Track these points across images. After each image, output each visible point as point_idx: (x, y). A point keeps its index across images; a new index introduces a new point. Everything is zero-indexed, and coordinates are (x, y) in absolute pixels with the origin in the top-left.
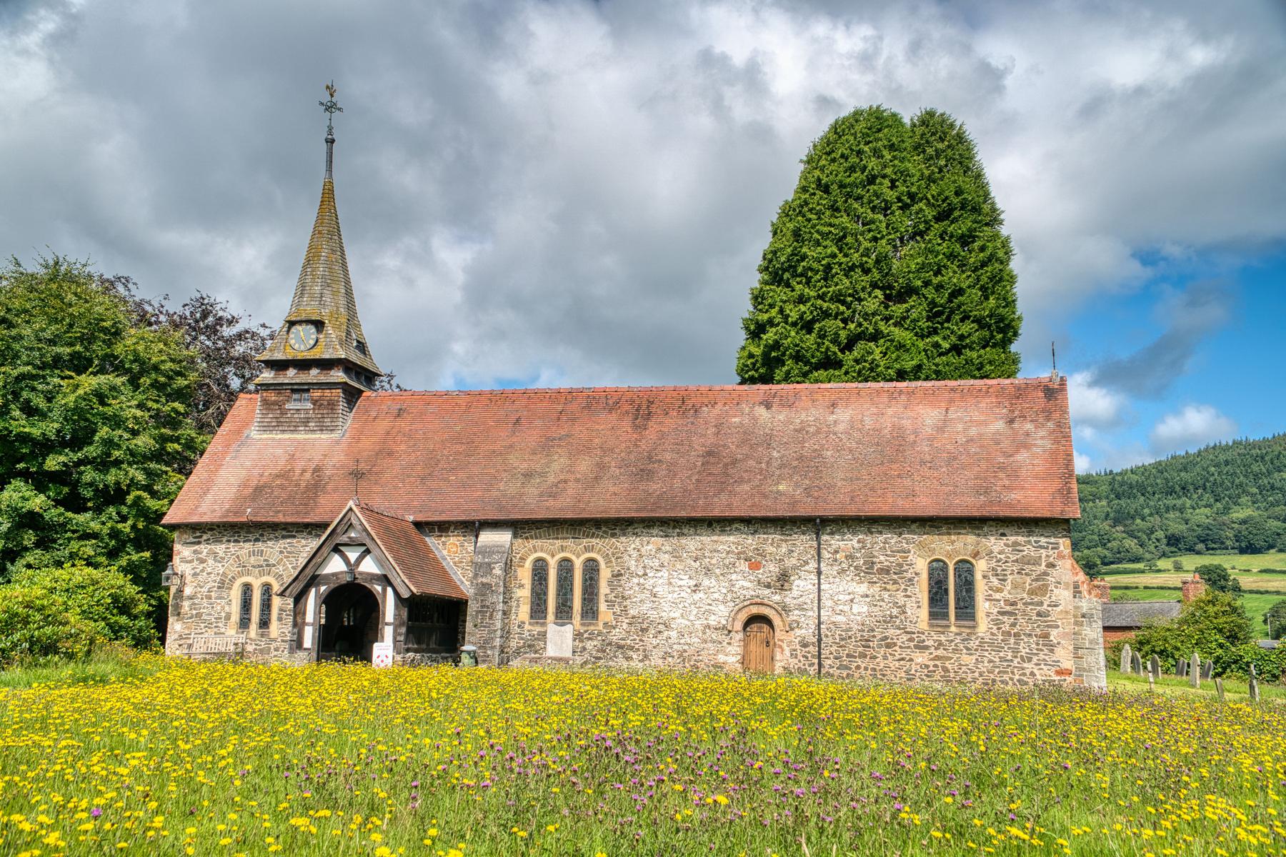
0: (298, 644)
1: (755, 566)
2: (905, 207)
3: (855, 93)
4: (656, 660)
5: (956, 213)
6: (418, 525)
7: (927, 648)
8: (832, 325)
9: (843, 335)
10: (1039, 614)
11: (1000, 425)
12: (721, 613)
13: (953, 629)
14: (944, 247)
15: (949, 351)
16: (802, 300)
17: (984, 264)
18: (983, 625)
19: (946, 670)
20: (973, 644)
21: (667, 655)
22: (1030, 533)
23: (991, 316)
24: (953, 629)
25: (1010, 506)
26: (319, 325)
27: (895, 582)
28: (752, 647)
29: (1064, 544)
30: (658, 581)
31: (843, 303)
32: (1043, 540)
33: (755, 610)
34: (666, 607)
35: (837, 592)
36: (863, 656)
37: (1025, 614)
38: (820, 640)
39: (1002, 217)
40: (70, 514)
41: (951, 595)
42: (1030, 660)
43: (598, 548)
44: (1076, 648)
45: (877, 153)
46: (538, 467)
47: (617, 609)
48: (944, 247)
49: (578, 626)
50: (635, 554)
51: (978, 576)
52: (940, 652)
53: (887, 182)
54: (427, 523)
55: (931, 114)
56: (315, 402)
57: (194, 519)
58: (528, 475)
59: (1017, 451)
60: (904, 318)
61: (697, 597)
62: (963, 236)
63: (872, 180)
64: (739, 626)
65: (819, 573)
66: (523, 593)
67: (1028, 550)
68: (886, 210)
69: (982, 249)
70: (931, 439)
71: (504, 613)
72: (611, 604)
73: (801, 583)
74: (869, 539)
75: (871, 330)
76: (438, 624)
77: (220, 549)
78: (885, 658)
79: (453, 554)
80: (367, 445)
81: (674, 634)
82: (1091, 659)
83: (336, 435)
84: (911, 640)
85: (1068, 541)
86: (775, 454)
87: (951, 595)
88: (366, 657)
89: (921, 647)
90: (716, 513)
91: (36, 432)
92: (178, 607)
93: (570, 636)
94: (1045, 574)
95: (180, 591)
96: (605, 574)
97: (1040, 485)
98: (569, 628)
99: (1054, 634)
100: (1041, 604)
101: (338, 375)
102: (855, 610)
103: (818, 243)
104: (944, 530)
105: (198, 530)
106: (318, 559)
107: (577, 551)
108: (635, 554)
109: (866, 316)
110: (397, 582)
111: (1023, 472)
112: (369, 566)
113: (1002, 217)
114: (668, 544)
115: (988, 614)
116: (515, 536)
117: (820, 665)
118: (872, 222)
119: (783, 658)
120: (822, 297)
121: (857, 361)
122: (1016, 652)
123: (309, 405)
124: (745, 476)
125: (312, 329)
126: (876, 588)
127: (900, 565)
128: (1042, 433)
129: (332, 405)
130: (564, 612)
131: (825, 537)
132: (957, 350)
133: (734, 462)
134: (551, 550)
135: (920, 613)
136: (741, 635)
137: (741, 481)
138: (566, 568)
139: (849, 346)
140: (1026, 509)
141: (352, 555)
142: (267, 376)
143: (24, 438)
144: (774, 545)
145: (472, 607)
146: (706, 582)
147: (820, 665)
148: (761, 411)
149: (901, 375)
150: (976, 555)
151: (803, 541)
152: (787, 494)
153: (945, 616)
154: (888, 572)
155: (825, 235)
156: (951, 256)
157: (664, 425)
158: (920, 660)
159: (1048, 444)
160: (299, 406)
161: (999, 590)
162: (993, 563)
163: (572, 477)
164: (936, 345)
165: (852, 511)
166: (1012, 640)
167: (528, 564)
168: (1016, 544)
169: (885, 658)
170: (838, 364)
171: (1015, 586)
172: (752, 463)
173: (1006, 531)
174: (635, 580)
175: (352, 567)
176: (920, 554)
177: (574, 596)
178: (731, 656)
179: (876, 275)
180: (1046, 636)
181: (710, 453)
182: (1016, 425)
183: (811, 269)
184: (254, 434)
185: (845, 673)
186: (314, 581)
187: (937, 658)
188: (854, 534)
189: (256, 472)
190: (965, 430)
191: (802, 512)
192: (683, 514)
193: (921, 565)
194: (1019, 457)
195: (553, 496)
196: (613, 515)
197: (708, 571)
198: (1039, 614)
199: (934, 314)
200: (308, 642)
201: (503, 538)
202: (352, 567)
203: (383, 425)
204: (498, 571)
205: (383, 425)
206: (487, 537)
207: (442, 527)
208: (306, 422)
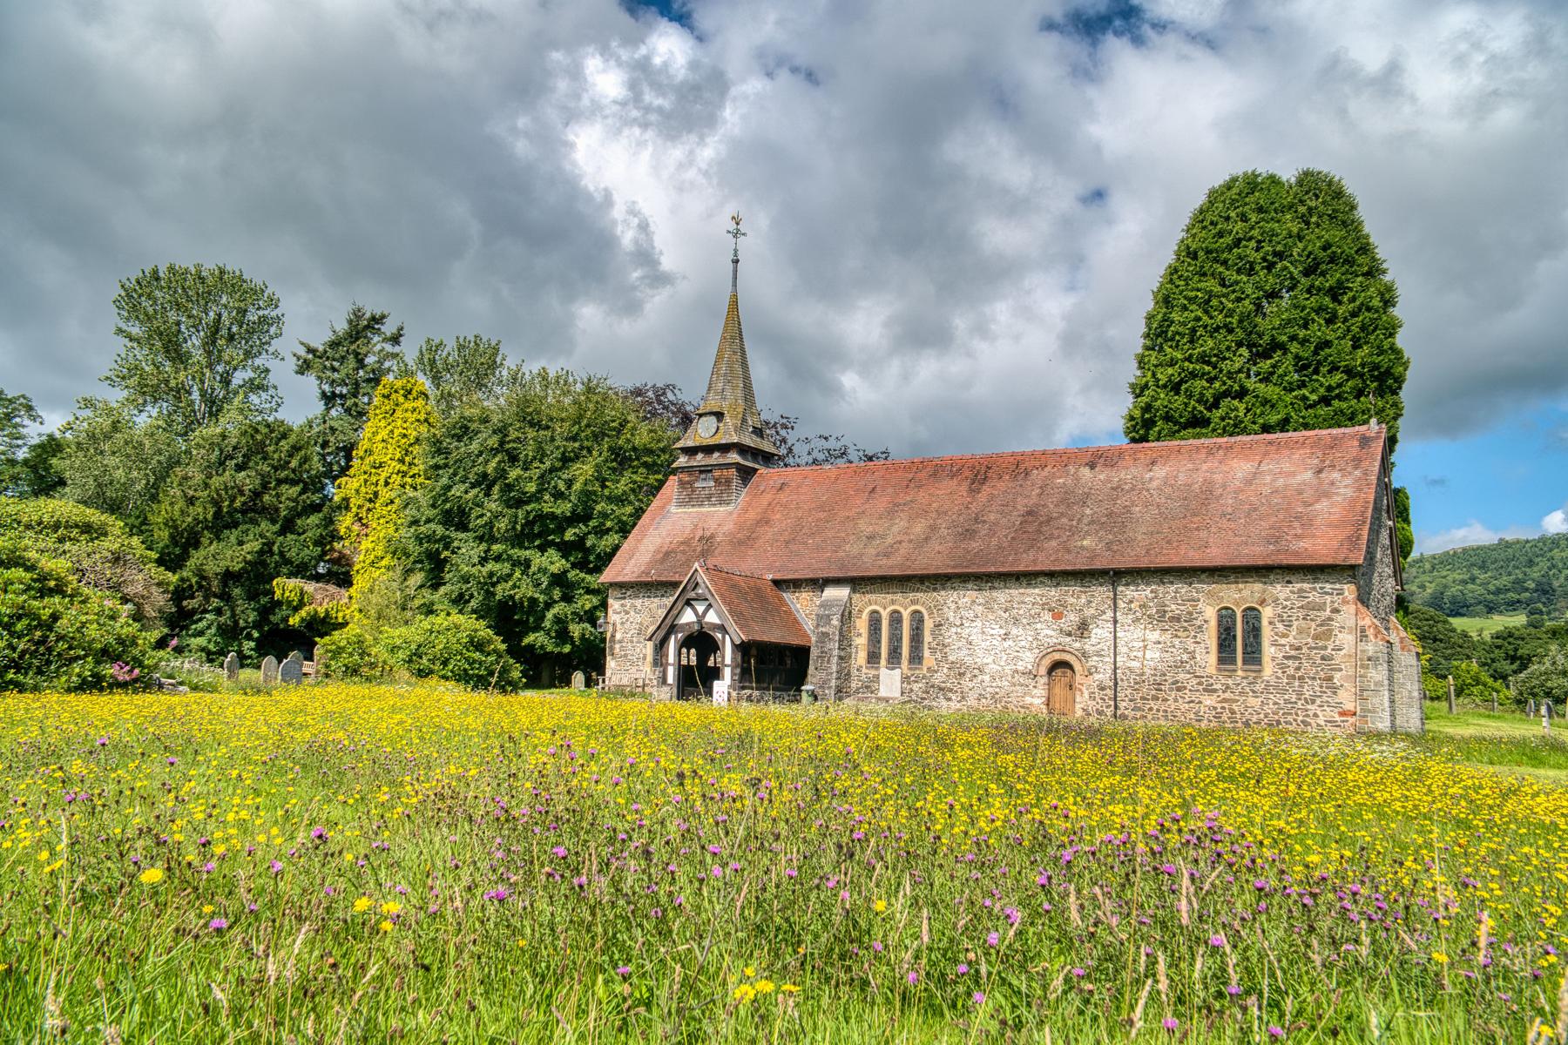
0: (664, 681)
1: (1058, 616)
2: (1270, 267)
3: (1215, 161)
4: (972, 702)
5: (1323, 267)
6: (776, 583)
7: (1215, 691)
8: (1200, 384)
9: (1209, 394)
10: (1323, 658)
11: (1308, 475)
12: (1028, 659)
13: (1240, 673)
14: (1313, 301)
15: (1319, 402)
16: (1172, 363)
17: (1354, 314)
18: (1268, 669)
19: (1233, 712)
20: (1259, 687)
21: (980, 697)
22: (1316, 580)
23: (1363, 365)
24: (1240, 673)
25: (1296, 554)
26: (719, 416)
27: (1186, 630)
28: (1057, 690)
29: (1349, 590)
30: (973, 631)
31: (1209, 363)
32: (1328, 586)
33: (1057, 656)
34: (980, 653)
35: (1133, 641)
36: (1155, 698)
37: (1309, 658)
38: (1116, 684)
39: (1385, 266)
40: (582, 575)
41: (1238, 641)
42: (1313, 702)
43: (922, 601)
44: (1362, 690)
45: (1244, 218)
46: (881, 531)
47: (939, 655)
48: (1313, 301)
49: (906, 671)
50: (953, 606)
51: (1265, 622)
52: (1228, 695)
53: (1253, 244)
54: (785, 581)
55: (1306, 173)
56: (716, 481)
57: (620, 579)
58: (871, 538)
59: (1317, 501)
60: (1272, 373)
61: (1006, 644)
62: (1331, 288)
63: (1237, 243)
64: (1043, 670)
65: (1115, 622)
66: (861, 641)
67: (1314, 597)
68: (1251, 271)
69: (1353, 300)
70: (1238, 491)
71: (841, 658)
72: (933, 651)
73: (1098, 631)
74: (1161, 589)
75: (1236, 387)
76: (778, 667)
77: (638, 602)
78: (1176, 700)
79: (803, 605)
80: (752, 515)
81: (987, 678)
82: (1376, 701)
83: (730, 508)
84: (1200, 684)
85: (1353, 587)
86: (1088, 511)
87: (1238, 641)
88: (709, 693)
89: (1210, 690)
90: (1021, 568)
91: (559, 511)
92: (612, 648)
93: (898, 678)
94: (1330, 619)
95: (613, 636)
96: (928, 624)
97: (1331, 533)
98: (898, 671)
99: (1337, 675)
100: (1325, 648)
101: (734, 457)
102: (1148, 656)
103: (1185, 308)
104: (1232, 579)
105: (628, 588)
106: (675, 612)
107: (905, 604)
108: (953, 606)
109: (1230, 375)
110: (730, 631)
111: (1318, 521)
112: (712, 618)
113: (1385, 266)
114: (981, 597)
115: (1273, 659)
116: (854, 591)
117: (1116, 707)
118: (1237, 283)
119: (1082, 701)
120: (1189, 359)
121: (1223, 419)
122: (1300, 694)
123: (712, 484)
124: (1056, 533)
125: (713, 419)
126: (1168, 635)
127: (1190, 613)
128: (1348, 481)
129: (728, 482)
130: (895, 655)
131: (1120, 588)
132: (1325, 401)
133: (1049, 520)
134: (883, 603)
135: (1209, 658)
136: (1045, 680)
137: (1052, 537)
138: (896, 619)
139: (1216, 405)
140: (1311, 557)
141: (700, 608)
142: (682, 460)
143: (553, 516)
144: (1075, 597)
145: (814, 653)
146: (1014, 631)
147: (1116, 707)
148: (1086, 471)
149: (1266, 429)
150: (1262, 602)
151: (1101, 593)
152: (1090, 547)
153: (1233, 661)
154: (1178, 619)
155: (1191, 300)
156: (1319, 310)
157: (998, 488)
158: (1208, 703)
159: (1349, 492)
160: (705, 484)
161: (1284, 636)
162: (1279, 610)
163: (906, 538)
164: (1304, 398)
165: (1144, 563)
166: (1297, 683)
167: (865, 615)
168: (1301, 590)
169: (1176, 700)
170: (1205, 422)
171: (1300, 632)
172: (1065, 520)
173: (1292, 578)
174: (954, 630)
175: (700, 618)
176: (1209, 602)
177: (905, 644)
178: (1036, 699)
179: (1240, 334)
180: (1330, 679)
181: (1030, 513)
182: (1323, 475)
183: (1178, 333)
184: (673, 509)
185: (1139, 714)
186: (673, 629)
187: (1225, 700)
188: (1148, 584)
189: (668, 540)
190: (1273, 481)
191: (1098, 565)
192: (993, 569)
193: (1210, 613)
194: (1318, 506)
195: (887, 555)
196: (932, 571)
197: (1016, 621)
198: (1323, 658)
199: (1301, 366)
200: (670, 680)
201: (843, 593)
202: (700, 618)
203: (767, 497)
204: (835, 622)
205: (767, 497)
206: (831, 593)
207: (796, 584)
208: (709, 498)
